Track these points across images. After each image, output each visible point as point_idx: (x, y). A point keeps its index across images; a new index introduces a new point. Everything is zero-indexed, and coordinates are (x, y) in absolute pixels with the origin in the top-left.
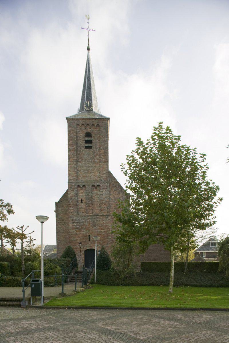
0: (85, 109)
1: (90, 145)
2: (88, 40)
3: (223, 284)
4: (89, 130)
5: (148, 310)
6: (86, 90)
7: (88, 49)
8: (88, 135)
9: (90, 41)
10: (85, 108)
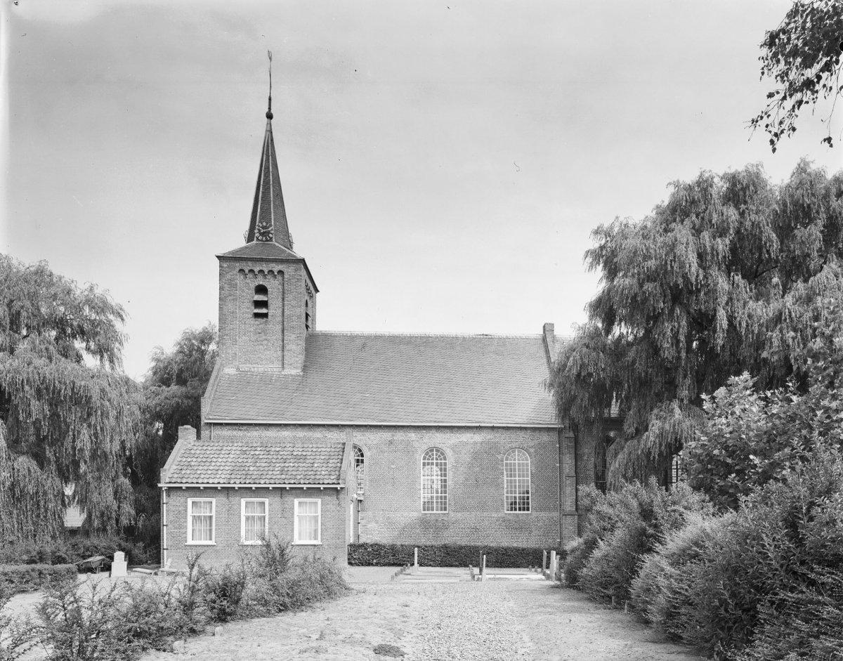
0: (257, 238)
1: (264, 311)
2: (270, 99)
3: (467, 480)
4: (260, 281)
5: (489, 551)
6: (258, 214)
7: (270, 116)
8: (261, 290)
9: (272, 101)
10: (257, 235)
